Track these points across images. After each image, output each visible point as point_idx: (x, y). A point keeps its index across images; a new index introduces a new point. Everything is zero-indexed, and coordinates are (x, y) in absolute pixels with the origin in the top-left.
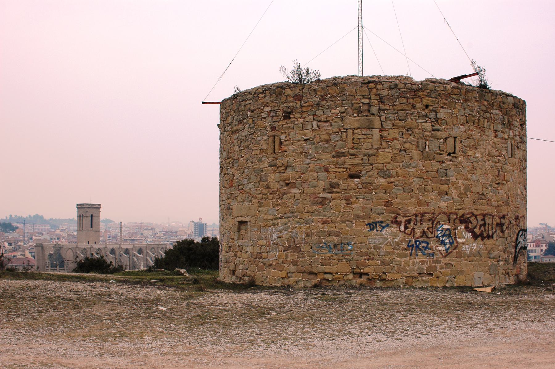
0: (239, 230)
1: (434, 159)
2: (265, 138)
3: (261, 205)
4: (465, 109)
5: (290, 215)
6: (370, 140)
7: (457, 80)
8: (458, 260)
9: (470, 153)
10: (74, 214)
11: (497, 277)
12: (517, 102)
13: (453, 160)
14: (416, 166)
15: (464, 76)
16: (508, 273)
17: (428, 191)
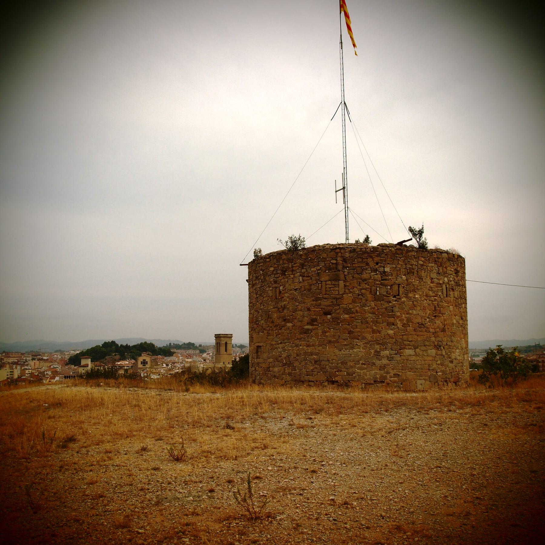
0: (257, 352)
1: (383, 300)
2: (271, 289)
3: (269, 334)
5: (286, 341)
6: (337, 289)
7: (400, 244)
8: (403, 371)
9: (411, 295)
10: (212, 341)
11: (436, 384)
12: (451, 256)
13: (398, 300)
14: (370, 306)
15: (405, 241)
16: (446, 381)
17: (380, 323)
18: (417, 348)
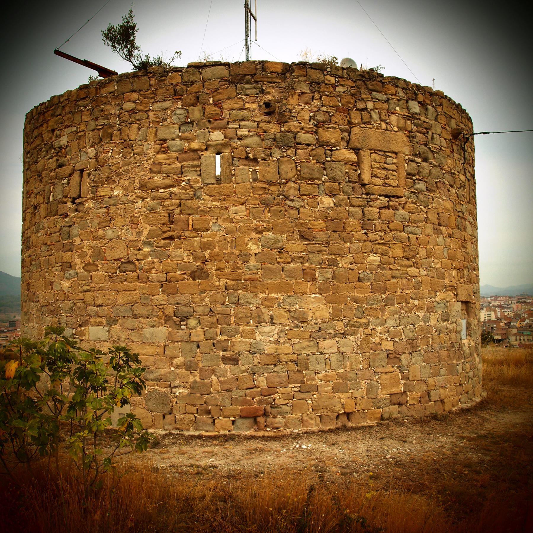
4: (96, 119)
9: (103, 192)
18: (115, 321)
